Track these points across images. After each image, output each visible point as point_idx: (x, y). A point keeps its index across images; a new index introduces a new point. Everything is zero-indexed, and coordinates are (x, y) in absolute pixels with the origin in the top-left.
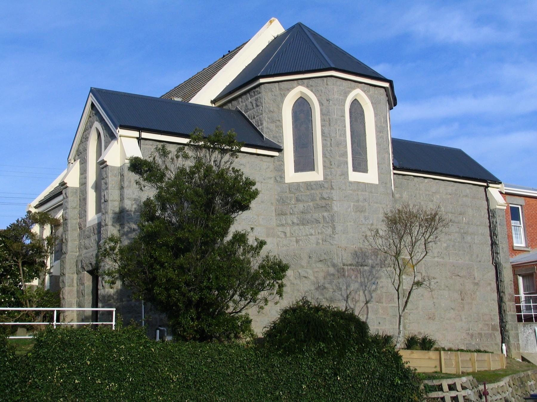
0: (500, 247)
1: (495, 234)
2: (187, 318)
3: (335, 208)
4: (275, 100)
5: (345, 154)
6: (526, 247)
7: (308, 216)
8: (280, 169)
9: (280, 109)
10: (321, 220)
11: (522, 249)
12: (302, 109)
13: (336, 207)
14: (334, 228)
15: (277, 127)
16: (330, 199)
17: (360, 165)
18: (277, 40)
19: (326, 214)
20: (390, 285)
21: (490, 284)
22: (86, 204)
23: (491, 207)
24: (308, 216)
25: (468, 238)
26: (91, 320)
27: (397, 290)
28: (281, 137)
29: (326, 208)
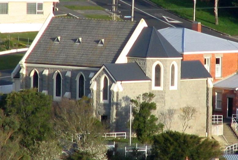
0: (209, 101)
1: (208, 99)
2: (155, 151)
3: (166, 98)
4: (150, 64)
5: (169, 82)
6: (221, 77)
7: (158, 100)
8: (150, 85)
9: (151, 67)
10: (161, 102)
11: (219, 78)
12: (158, 68)
13: (166, 98)
14: (165, 104)
15: (151, 73)
16: (165, 96)
17: (172, 84)
18: (144, 29)
19: (163, 100)
20: (181, 126)
21: (205, 113)
22: (100, 99)
23: (208, 87)
24: (158, 100)
25: (200, 98)
26: (147, 155)
27: (183, 127)
28: (151, 76)
29: (163, 98)
